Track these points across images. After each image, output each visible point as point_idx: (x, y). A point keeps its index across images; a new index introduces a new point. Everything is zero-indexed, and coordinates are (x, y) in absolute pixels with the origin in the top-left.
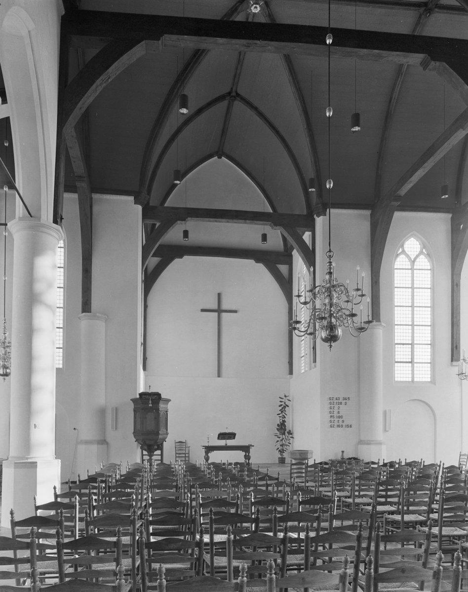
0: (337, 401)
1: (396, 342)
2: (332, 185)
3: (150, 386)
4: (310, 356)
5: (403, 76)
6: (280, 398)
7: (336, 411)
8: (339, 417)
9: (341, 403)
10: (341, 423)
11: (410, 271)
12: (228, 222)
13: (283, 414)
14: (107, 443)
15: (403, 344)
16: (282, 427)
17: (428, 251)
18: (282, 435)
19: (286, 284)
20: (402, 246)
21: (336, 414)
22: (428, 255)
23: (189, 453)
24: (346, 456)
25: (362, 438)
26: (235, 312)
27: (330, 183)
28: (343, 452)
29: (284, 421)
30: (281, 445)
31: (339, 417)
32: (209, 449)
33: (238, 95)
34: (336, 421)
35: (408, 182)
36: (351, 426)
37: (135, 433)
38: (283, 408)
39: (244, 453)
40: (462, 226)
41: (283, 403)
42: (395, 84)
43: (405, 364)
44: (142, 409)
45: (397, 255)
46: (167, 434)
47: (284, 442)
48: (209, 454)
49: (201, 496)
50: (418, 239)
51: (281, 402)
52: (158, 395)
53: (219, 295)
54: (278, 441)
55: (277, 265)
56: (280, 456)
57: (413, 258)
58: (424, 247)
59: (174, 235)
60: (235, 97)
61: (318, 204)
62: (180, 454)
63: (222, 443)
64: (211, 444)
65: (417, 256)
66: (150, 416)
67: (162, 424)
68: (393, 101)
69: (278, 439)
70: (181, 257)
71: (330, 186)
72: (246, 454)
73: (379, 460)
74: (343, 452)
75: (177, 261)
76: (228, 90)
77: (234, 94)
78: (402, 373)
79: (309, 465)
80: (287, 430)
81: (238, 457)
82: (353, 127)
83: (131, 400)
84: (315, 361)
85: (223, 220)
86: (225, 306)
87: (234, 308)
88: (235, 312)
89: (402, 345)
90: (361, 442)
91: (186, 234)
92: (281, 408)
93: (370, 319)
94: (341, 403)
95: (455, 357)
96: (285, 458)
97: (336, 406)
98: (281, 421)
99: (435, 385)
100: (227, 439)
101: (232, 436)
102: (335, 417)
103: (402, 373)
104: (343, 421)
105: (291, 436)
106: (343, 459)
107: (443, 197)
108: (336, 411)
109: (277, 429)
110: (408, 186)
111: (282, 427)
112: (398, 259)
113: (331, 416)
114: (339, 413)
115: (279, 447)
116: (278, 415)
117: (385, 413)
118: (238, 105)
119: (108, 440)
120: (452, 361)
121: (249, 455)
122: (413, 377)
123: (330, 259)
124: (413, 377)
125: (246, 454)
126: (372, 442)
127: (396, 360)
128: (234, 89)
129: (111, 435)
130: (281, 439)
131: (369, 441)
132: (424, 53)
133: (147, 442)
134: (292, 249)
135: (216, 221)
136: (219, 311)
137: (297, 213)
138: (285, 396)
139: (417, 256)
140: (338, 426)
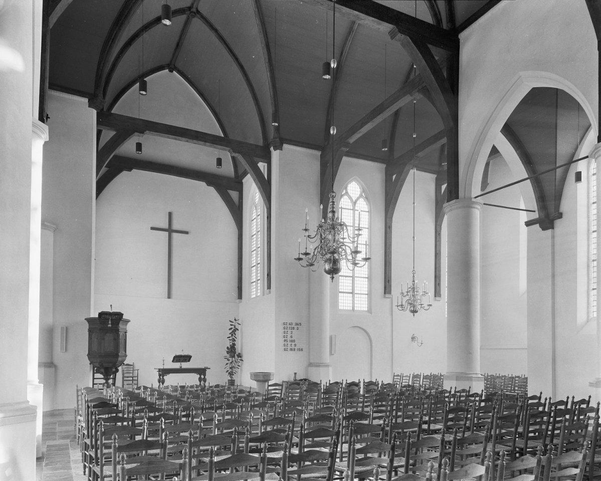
0: (291, 326)
2: (335, 132)
3: (111, 306)
4: (264, 281)
5: (354, 33)
6: (230, 321)
7: (289, 335)
8: (292, 341)
10: (293, 347)
11: (352, 211)
12: (187, 141)
13: (233, 337)
14: (55, 367)
15: (346, 276)
16: (232, 350)
17: (367, 195)
18: (232, 357)
20: (346, 188)
21: (289, 339)
22: (367, 198)
23: (137, 377)
24: (298, 378)
25: (312, 361)
26: (187, 233)
27: (334, 130)
28: (295, 374)
29: (234, 345)
30: (230, 368)
31: (292, 341)
32: (164, 372)
33: (198, 12)
34: (289, 345)
35: (358, 132)
36: (302, 350)
37: (90, 355)
38: (233, 331)
39: (199, 376)
40: (394, 177)
41: (233, 327)
42: (347, 39)
44: (100, 330)
45: (342, 196)
46: (126, 356)
47: (233, 365)
48: (165, 377)
49: (163, 421)
50: (359, 183)
51: (231, 325)
52: (120, 315)
53: (170, 214)
54: (227, 364)
57: (354, 200)
58: (364, 191)
59: (128, 148)
60: (195, 13)
61: (276, 138)
62: (128, 377)
63: (177, 365)
64: (166, 367)
65: (358, 199)
66: (109, 337)
67: (121, 346)
69: (228, 362)
70: (130, 170)
71: (334, 133)
72: (200, 377)
73: (470, 387)
75: (125, 173)
76: (189, 5)
77: (194, 10)
79: (471, 393)
81: (192, 380)
82: (324, 75)
83: (85, 319)
84: (269, 287)
85: (184, 139)
86: (175, 226)
87: (187, 230)
88: (187, 233)
89: (344, 278)
90: (310, 365)
91: (139, 147)
92: (231, 331)
96: (234, 380)
97: (289, 331)
98: (231, 344)
100: (182, 362)
101: (187, 358)
102: (289, 341)
103: (344, 302)
104: (295, 345)
105: (239, 358)
106: (295, 380)
108: (289, 335)
109: (228, 352)
110: (357, 136)
111: (232, 350)
112: (342, 200)
113: (285, 340)
114: (291, 337)
117: (331, 338)
118: (196, 22)
119: (56, 362)
120: (385, 293)
121: (204, 378)
123: (333, 199)
125: (200, 377)
127: (340, 291)
128: (195, 5)
129: (59, 356)
130: (230, 361)
131: (319, 363)
132: (392, 24)
133: (106, 365)
134: (245, 174)
135: (176, 139)
136: (170, 230)
137: (252, 142)
138: (235, 320)
139: (358, 199)
140: (291, 350)
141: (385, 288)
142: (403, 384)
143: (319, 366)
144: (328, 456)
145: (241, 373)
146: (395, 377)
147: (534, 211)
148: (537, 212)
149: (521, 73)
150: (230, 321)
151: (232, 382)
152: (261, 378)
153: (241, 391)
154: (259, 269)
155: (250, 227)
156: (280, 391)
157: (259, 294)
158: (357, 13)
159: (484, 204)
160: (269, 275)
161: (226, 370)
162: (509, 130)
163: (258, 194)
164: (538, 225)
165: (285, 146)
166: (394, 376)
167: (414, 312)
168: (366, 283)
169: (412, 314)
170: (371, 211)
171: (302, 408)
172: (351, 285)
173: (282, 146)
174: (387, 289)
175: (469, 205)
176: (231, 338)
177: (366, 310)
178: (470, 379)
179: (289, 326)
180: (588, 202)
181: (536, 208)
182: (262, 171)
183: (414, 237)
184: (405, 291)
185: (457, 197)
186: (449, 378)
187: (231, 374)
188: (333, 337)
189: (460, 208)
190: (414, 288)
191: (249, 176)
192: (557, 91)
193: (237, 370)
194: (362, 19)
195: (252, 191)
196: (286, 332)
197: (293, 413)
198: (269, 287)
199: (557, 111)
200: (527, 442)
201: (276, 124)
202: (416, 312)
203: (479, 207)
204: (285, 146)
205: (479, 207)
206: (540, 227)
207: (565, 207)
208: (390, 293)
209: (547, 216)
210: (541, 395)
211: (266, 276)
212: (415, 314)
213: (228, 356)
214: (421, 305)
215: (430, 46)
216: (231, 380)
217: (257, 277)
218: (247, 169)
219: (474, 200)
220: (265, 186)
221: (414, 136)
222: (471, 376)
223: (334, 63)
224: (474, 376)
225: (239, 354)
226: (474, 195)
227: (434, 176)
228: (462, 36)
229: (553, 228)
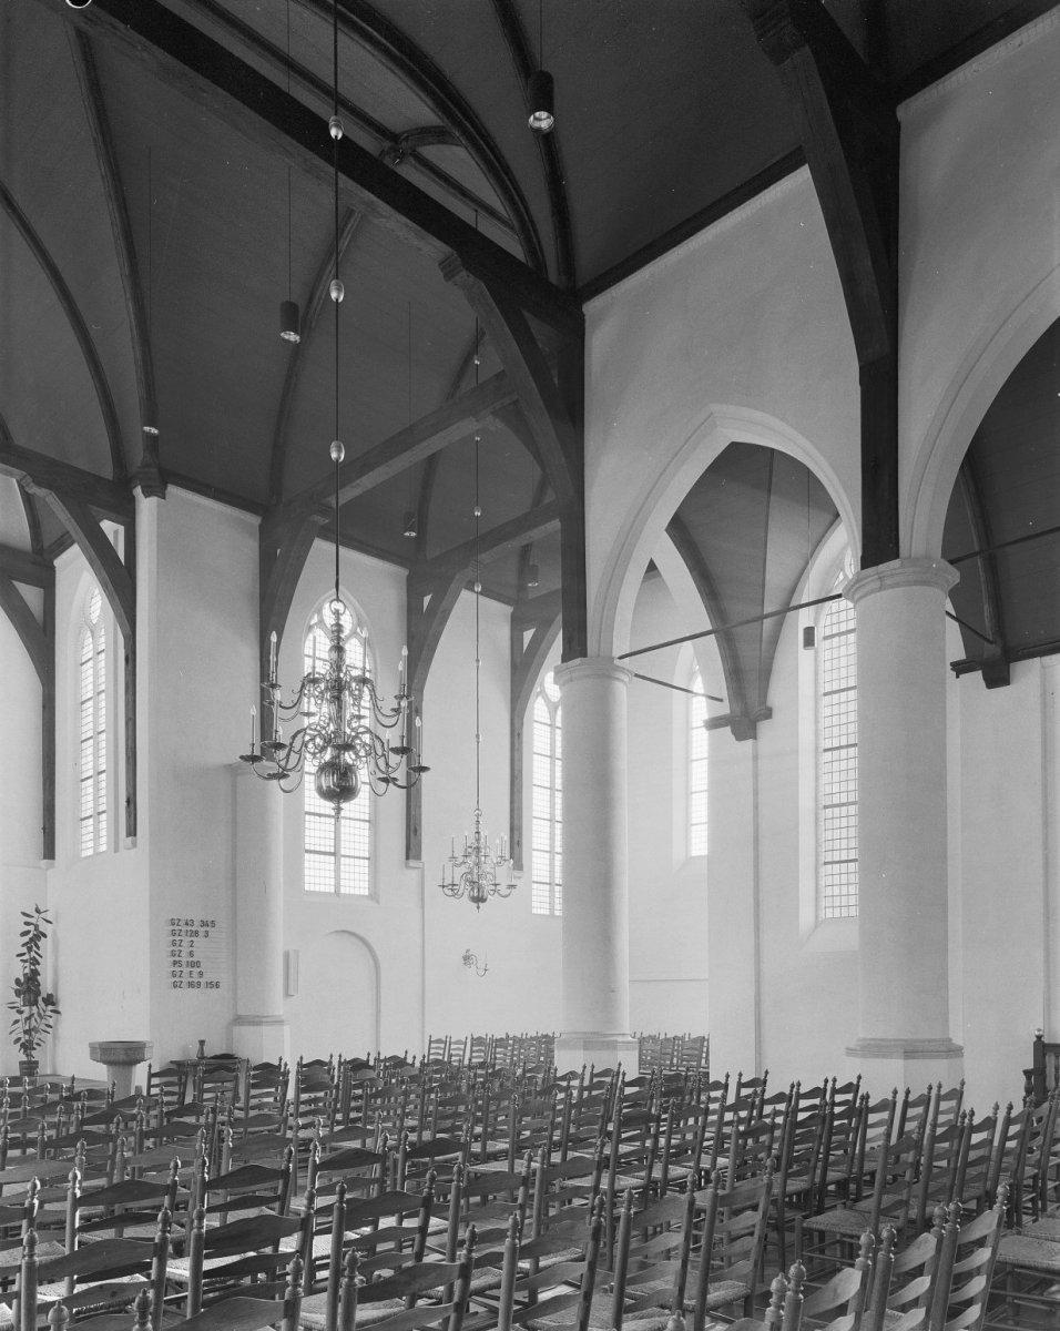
1: (307, 809)
7: (185, 950)
9: (197, 932)
15: (320, 815)
19: (40, 638)
24: (210, 1051)
25: (241, 1012)
28: (202, 1043)
29: (35, 973)
30: (25, 1032)
36: (218, 985)
40: (427, 599)
41: (31, 928)
43: (322, 856)
51: (27, 924)
54: (16, 1022)
55: (15, 583)
56: (25, 1059)
68: (315, 301)
69: (18, 1016)
74: (202, 1043)
78: (317, 876)
80: (44, 995)
84: (132, 831)
90: (239, 1020)
92: (26, 939)
93: (257, 752)
94: (197, 932)
95: (412, 853)
96: (37, 1062)
98: (27, 971)
99: (378, 902)
103: (317, 876)
104: (201, 974)
105: (50, 1007)
107: (407, 534)
108: (185, 950)
109: (18, 993)
113: (175, 963)
114: (191, 954)
115: (21, 1035)
116: (18, 955)
117: (287, 956)
120: (408, 858)
122: (337, 886)
124: (337, 886)
126: (264, 1020)
127: (307, 847)
130: (25, 1015)
134: (62, 544)
138: (38, 911)
140: (191, 985)
141: (408, 848)
142: (474, 1060)
143: (259, 1023)
144: (456, 1274)
145: (55, 1045)
146: (433, 1045)
147: (721, 700)
148: (726, 702)
149: (715, 407)
150: (24, 914)
151: (30, 1067)
152: (122, 1057)
153: (55, 1087)
154: (103, 784)
155: (78, 681)
156: (152, 1083)
157: (103, 848)
158: (372, 197)
159: (636, 675)
160: (131, 802)
161: (14, 1036)
162: (679, 529)
163: (99, 597)
164: (728, 729)
165: (172, 490)
166: (430, 1042)
167: (479, 900)
168: (367, 833)
169: (476, 905)
170: (376, 669)
171: (198, 1120)
172: (333, 836)
173: (166, 488)
174: (412, 849)
175: (606, 672)
176: (26, 957)
177: (367, 894)
178: (612, 1046)
179: (184, 928)
180: (816, 692)
181: (724, 694)
182: (111, 538)
183: (478, 736)
184: (459, 853)
185: (584, 654)
186: (566, 1045)
187: (27, 1047)
188: (292, 955)
189: (588, 676)
190: (478, 848)
191: (75, 549)
192: (772, 453)
193: (43, 1036)
194: (382, 216)
195: (80, 589)
196: (178, 943)
197: (286, 1151)
198: (132, 831)
199: (769, 497)
200: (785, 1182)
201: (154, 431)
202: (482, 900)
203: (627, 679)
204: (172, 490)
205: (627, 679)
206: (734, 732)
207: (776, 697)
208: (418, 857)
209: (746, 713)
210: (727, 1080)
211: (123, 803)
212: (481, 905)
213: (19, 1001)
214: (496, 885)
215: (527, 314)
216: (29, 1062)
217: (96, 804)
218: (72, 533)
219: (617, 662)
220: (120, 581)
221: (478, 513)
222: (615, 1038)
223: (339, 290)
224: (620, 1039)
225: (50, 996)
226: (617, 653)
227: (509, 610)
228: (591, 308)
229: (755, 737)
